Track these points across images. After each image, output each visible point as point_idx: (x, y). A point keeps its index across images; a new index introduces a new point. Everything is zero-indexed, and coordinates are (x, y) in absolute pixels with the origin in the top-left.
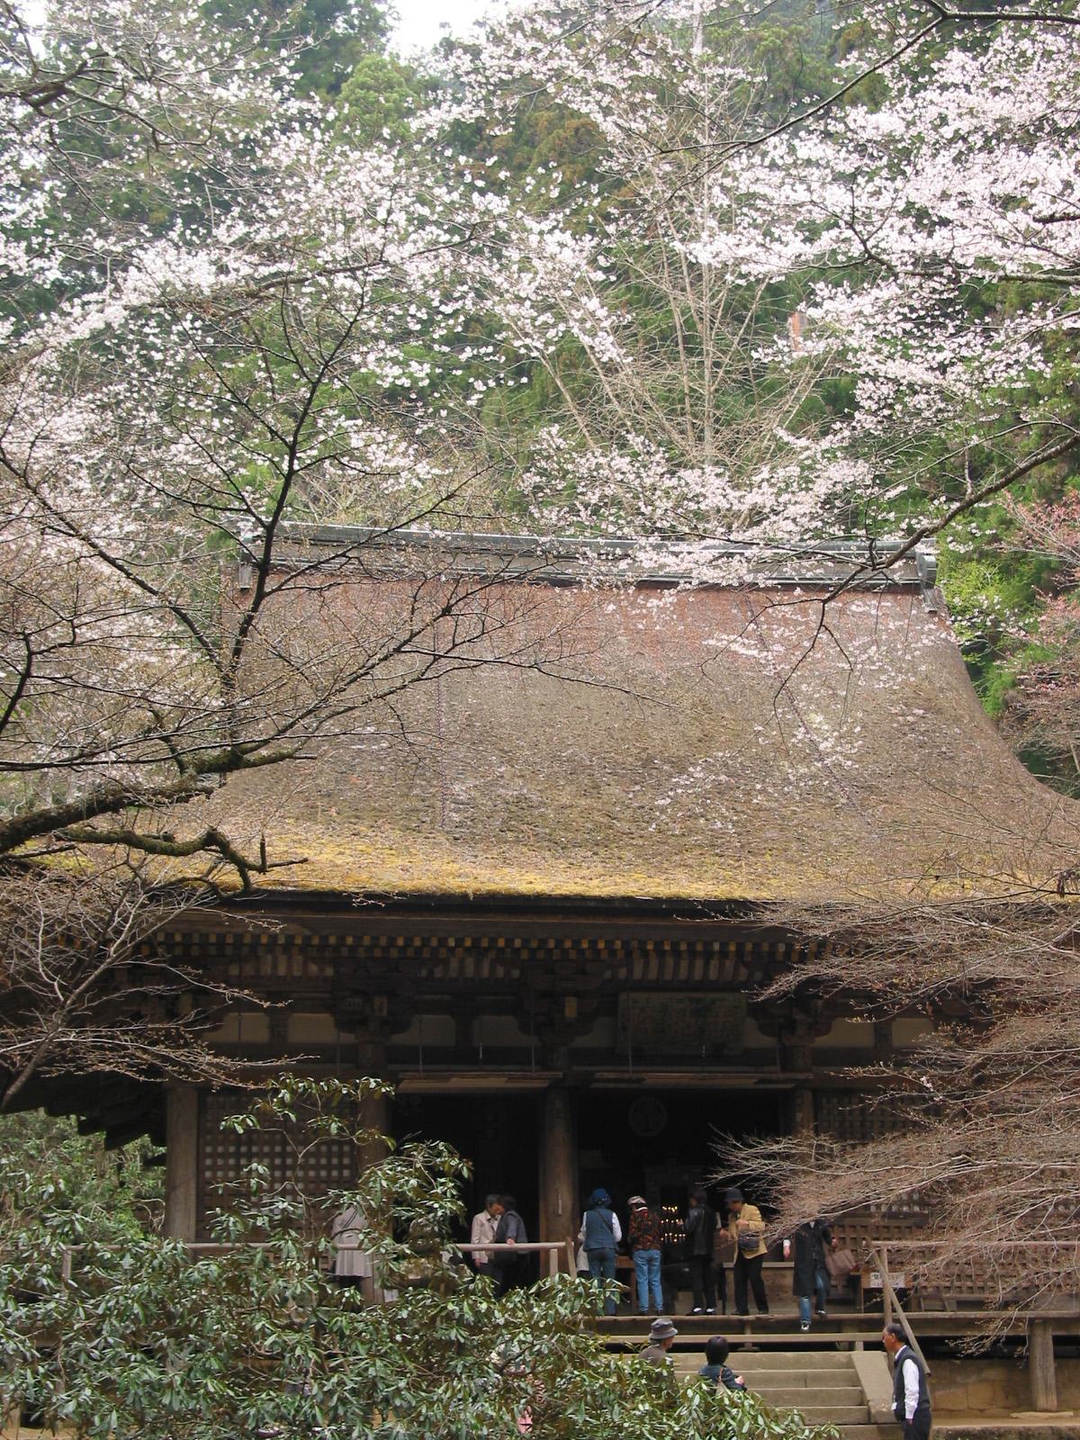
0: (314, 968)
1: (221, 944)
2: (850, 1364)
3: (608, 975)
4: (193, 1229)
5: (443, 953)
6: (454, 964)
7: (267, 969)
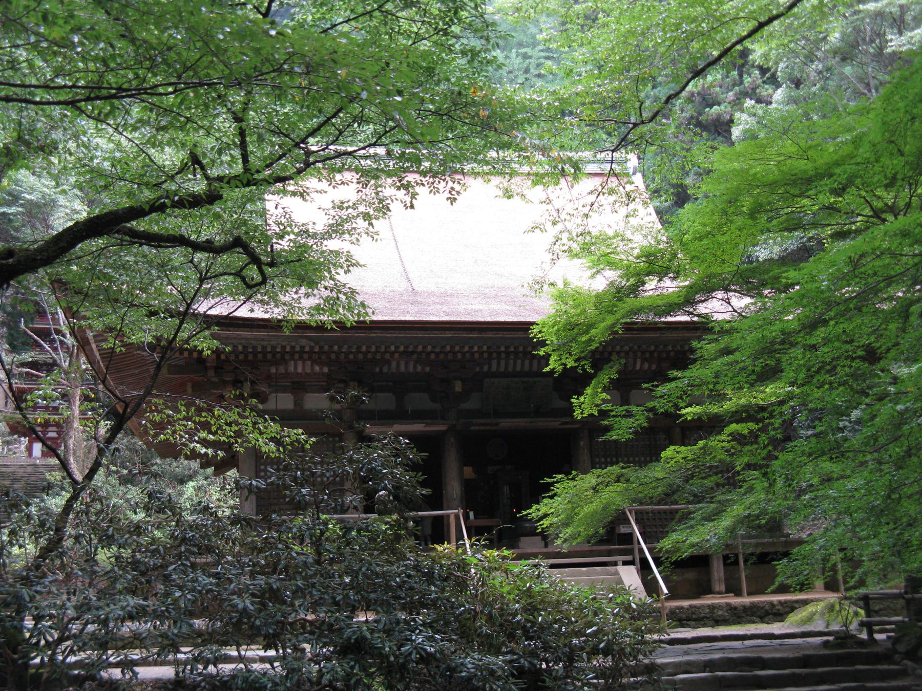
0: (317, 368)
1: (264, 353)
2: (617, 573)
3: (478, 369)
4: (255, 510)
5: (387, 356)
6: (394, 364)
7: (291, 369)
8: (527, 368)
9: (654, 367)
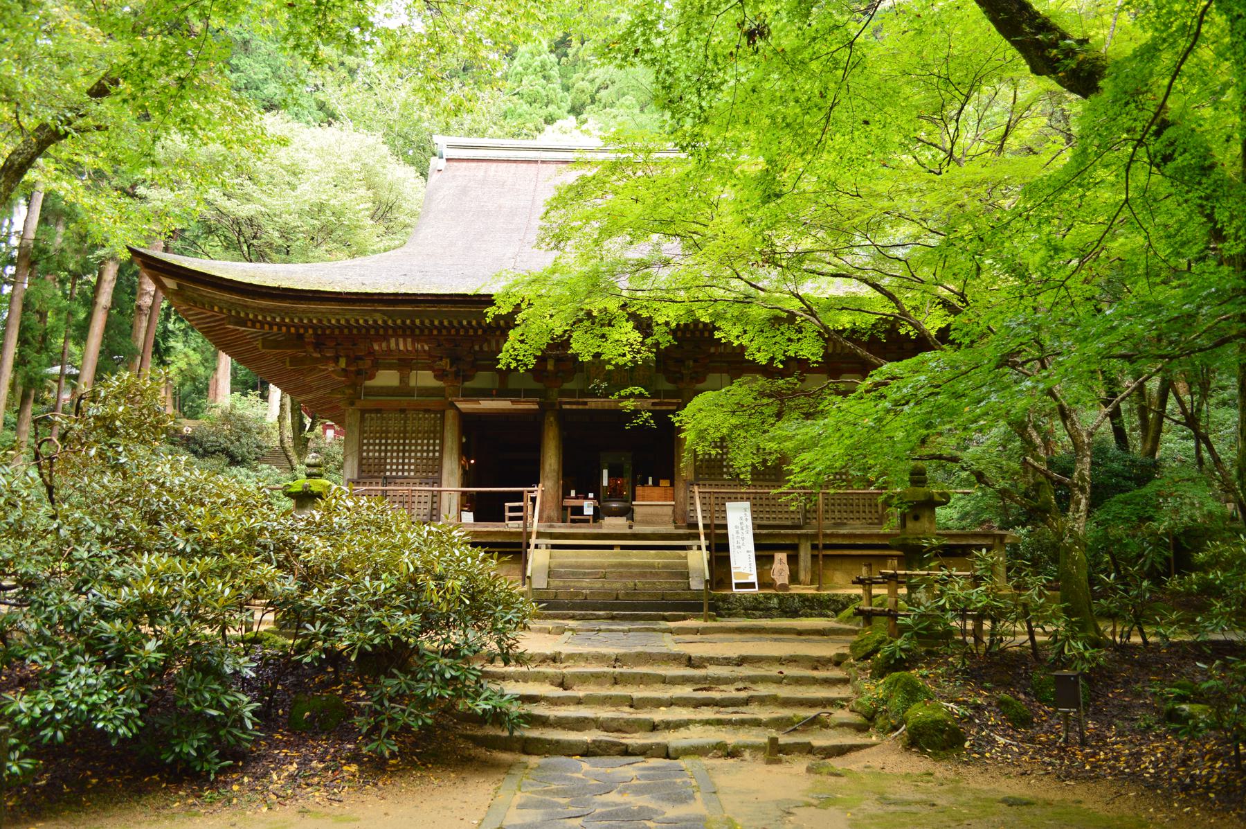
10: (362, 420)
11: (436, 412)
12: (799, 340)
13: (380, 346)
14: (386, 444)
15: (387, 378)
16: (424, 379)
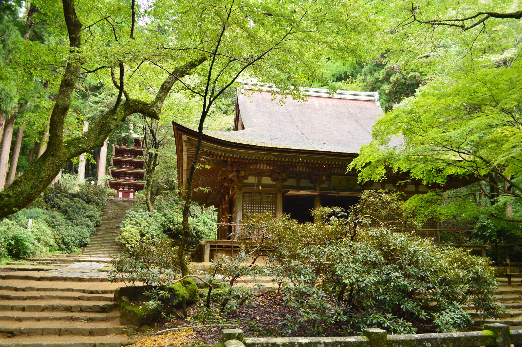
8: (336, 171)
9: (272, 168)
10: (243, 196)
11: (273, 194)
12: (438, 176)
13: (270, 168)
14: (254, 207)
15: (252, 180)
16: (267, 180)
